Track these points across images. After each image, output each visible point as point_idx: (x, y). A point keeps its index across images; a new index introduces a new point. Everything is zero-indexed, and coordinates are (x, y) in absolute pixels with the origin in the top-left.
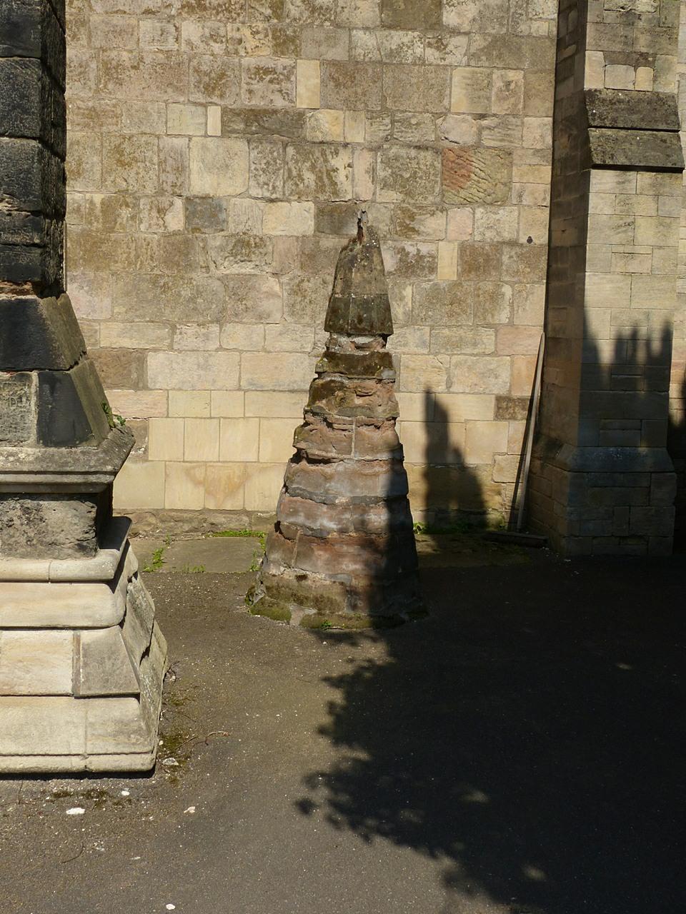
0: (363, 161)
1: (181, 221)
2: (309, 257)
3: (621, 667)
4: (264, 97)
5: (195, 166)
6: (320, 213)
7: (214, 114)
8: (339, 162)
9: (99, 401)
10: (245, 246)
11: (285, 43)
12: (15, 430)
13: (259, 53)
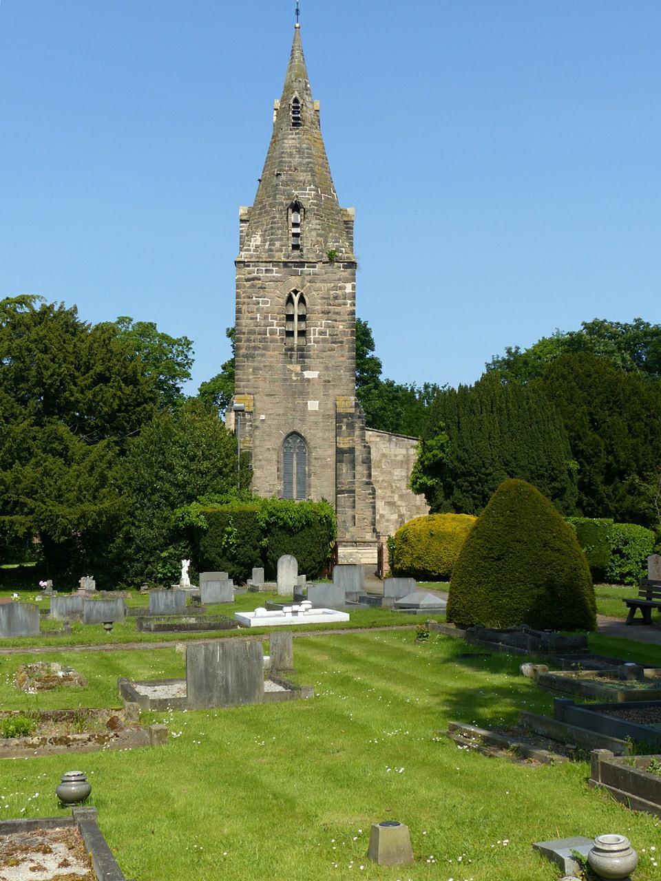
0: (404, 508)
1: (69, 830)
2: (397, 522)
3: (25, 566)
4: (390, 500)
5: (380, 509)
6: (399, 515)
7: (383, 502)
8: (401, 508)
9: (274, 628)
10: (388, 521)
11: (393, 492)
12: (517, 407)
13: (389, 494)
